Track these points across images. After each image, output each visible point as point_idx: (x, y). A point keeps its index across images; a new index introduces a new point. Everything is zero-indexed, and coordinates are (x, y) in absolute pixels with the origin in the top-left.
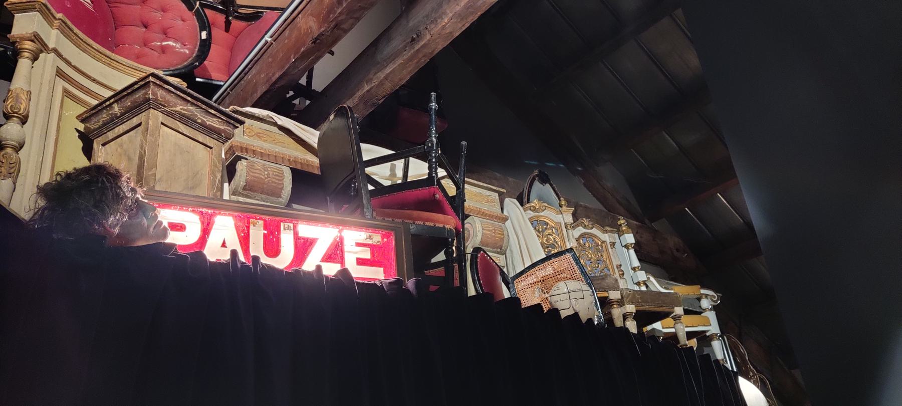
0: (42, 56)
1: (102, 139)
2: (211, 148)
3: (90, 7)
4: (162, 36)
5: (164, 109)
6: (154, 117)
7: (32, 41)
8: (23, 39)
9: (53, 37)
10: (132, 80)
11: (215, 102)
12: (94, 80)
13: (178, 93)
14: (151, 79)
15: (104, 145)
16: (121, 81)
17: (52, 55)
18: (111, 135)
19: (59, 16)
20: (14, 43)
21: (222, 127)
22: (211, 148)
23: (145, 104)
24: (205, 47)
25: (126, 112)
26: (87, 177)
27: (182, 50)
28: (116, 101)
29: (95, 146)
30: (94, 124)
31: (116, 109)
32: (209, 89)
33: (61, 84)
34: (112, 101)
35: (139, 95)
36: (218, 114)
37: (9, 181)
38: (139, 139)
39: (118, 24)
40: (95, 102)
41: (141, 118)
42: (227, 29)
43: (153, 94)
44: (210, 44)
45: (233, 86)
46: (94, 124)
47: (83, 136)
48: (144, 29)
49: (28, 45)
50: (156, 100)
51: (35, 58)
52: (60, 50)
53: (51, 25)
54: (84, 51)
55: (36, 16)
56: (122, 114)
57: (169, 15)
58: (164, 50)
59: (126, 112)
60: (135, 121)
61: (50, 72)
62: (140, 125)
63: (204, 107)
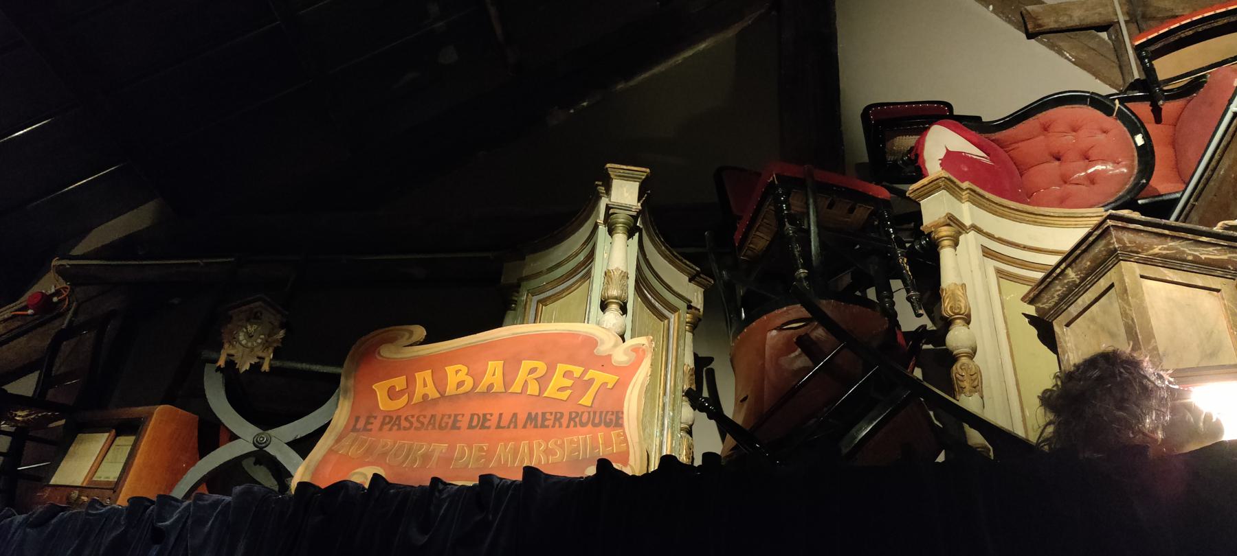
0: (962, 238)
1: (1063, 318)
2: (1218, 291)
3: (988, 161)
4: (1082, 163)
5: (1137, 256)
6: (1130, 270)
7: (948, 225)
8: (938, 226)
9: (967, 212)
10: (1080, 233)
11: (1177, 220)
12: (1025, 248)
13: (1149, 229)
14: (1109, 222)
15: (1068, 325)
16: (1066, 237)
17: (972, 233)
18: (1073, 310)
19: (966, 185)
20: (929, 234)
21: (1225, 257)
22: (1218, 291)
23: (1113, 257)
24: (1146, 155)
25: (1088, 275)
26: (1096, 373)
27: (1115, 170)
28: (1069, 265)
29: (1057, 329)
30: (1047, 302)
31: (1072, 275)
32: (1161, 208)
33: (991, 264)
34: (1063, 266)
35: (1100, 247)
36: (1213, 241)
37: (976, 395)
38: (1116, 305)
39: (1022, 168)
40: (1039, 275)
41: (1111, 276)
42: (1158, 119)
43: (1119, 241)
44: (1152, 147)
45: (1198, 193)
46: (1047, 302)
47: (1033, 320)
48: (1057, 163)
49: (945, 231)
50: (1124, 248)
51: (956, 244)
52: (978, 225)
53: (960, 199)
54: (1002, 216)
55: (942, 196)
56: (1083, 279)
57: (1082, 133)
58: (1092, 179)
59: (1088, 275)
60: (1103, 283)
61: (976, 254)
62: (1112, 286)
63: (1190, 236)
